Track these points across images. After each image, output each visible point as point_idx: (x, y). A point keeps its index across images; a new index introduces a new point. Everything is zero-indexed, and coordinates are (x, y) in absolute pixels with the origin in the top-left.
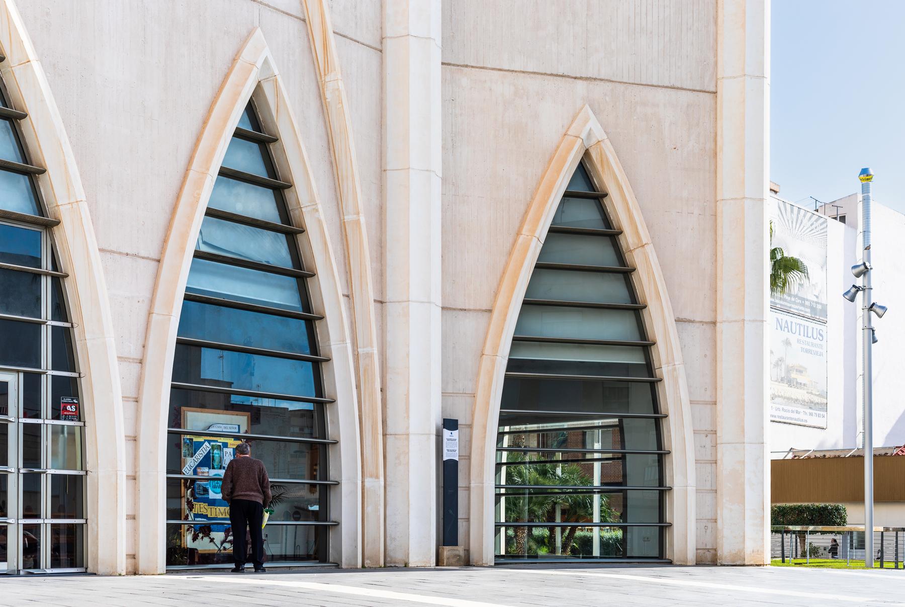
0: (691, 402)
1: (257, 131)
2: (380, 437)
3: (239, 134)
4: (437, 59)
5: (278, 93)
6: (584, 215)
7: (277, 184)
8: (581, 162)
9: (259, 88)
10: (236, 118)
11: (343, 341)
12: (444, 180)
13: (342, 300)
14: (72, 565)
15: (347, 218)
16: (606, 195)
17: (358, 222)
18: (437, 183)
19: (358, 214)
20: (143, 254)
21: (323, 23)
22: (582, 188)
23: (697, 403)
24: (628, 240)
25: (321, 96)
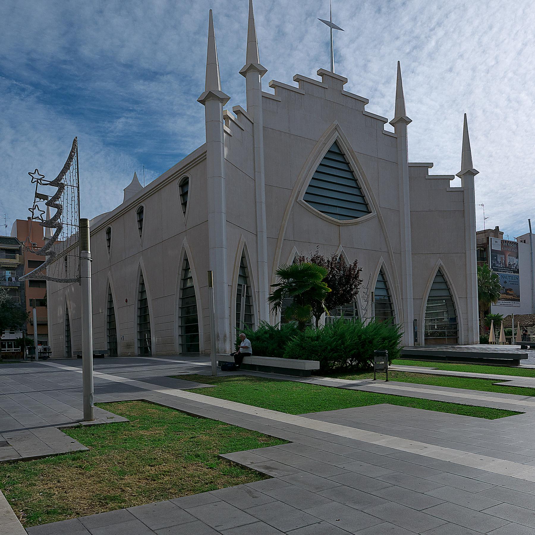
1: (382, 273)
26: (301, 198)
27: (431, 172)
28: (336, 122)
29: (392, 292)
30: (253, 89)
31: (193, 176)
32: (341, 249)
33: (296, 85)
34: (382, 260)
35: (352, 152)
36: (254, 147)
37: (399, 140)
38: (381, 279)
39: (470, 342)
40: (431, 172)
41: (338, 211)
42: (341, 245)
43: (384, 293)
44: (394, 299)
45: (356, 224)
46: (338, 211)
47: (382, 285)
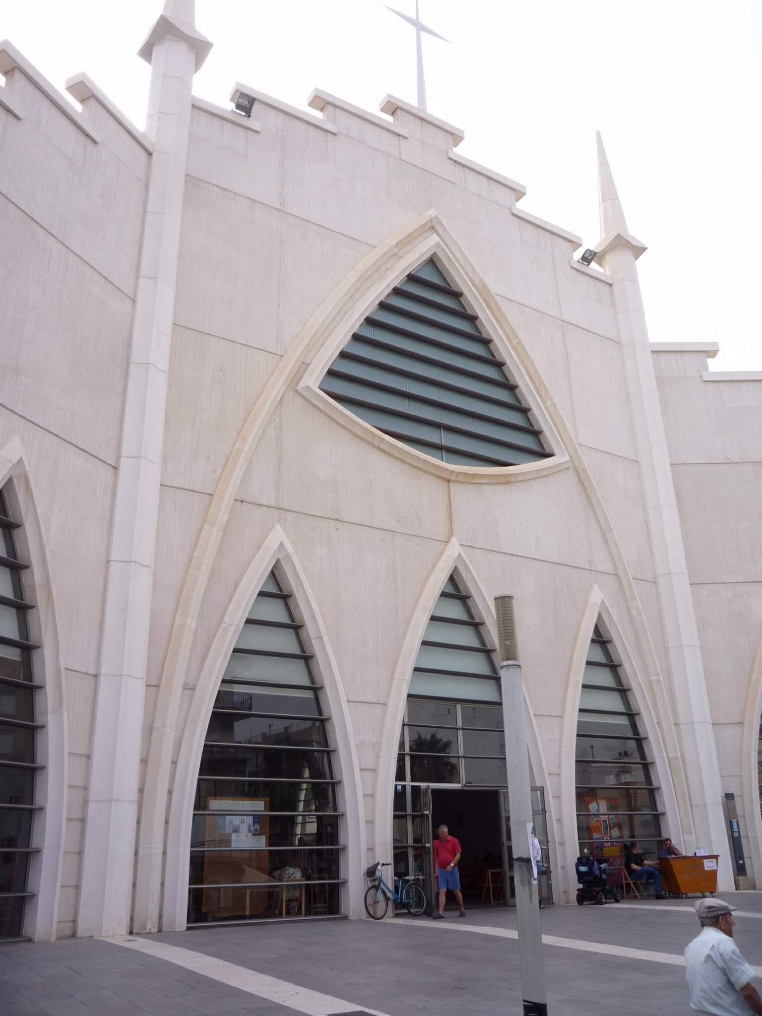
0: (361, 769)
1: (600, 639)
2: (689, 808)
3: (593, 641)
4: (687, 583)
5: (610, 616)
6: (274, 612)
7: (613, 667)
8: (272, 572)
9: (600, 617)
10: (589, 634)
11: (661, 751)
12: (702, 649)
13: (673, 727)
14: (331, 913)
15: (653, 678)
16: (27, 567)
17: (659, 681)
18: (698, 650)
19: (658, 675)
20: (554, 714)
21: (627, 574)
22: (272, 589)
23: (365, 770)
24: (310, 630)
25: (629, 613)
26: (314, 378)
27: (715, 366)
28: (432, 213)
29: (641, 701)
30: (170, 91)
31: (276, 572)
32: (454, 549)
33: (317, 115)
34: (597, 596)
35: (484, 290)
36: (145, 211)
37: (618, 296)
38: (600, 658)
39: (315, 856)
40: (715, 366)
41: (446, 439)
42: (454, 540)
43: (612, 702)
44: (648, 725)
45: (506, 481)
46: (446, 439)
47: (604, 678)
